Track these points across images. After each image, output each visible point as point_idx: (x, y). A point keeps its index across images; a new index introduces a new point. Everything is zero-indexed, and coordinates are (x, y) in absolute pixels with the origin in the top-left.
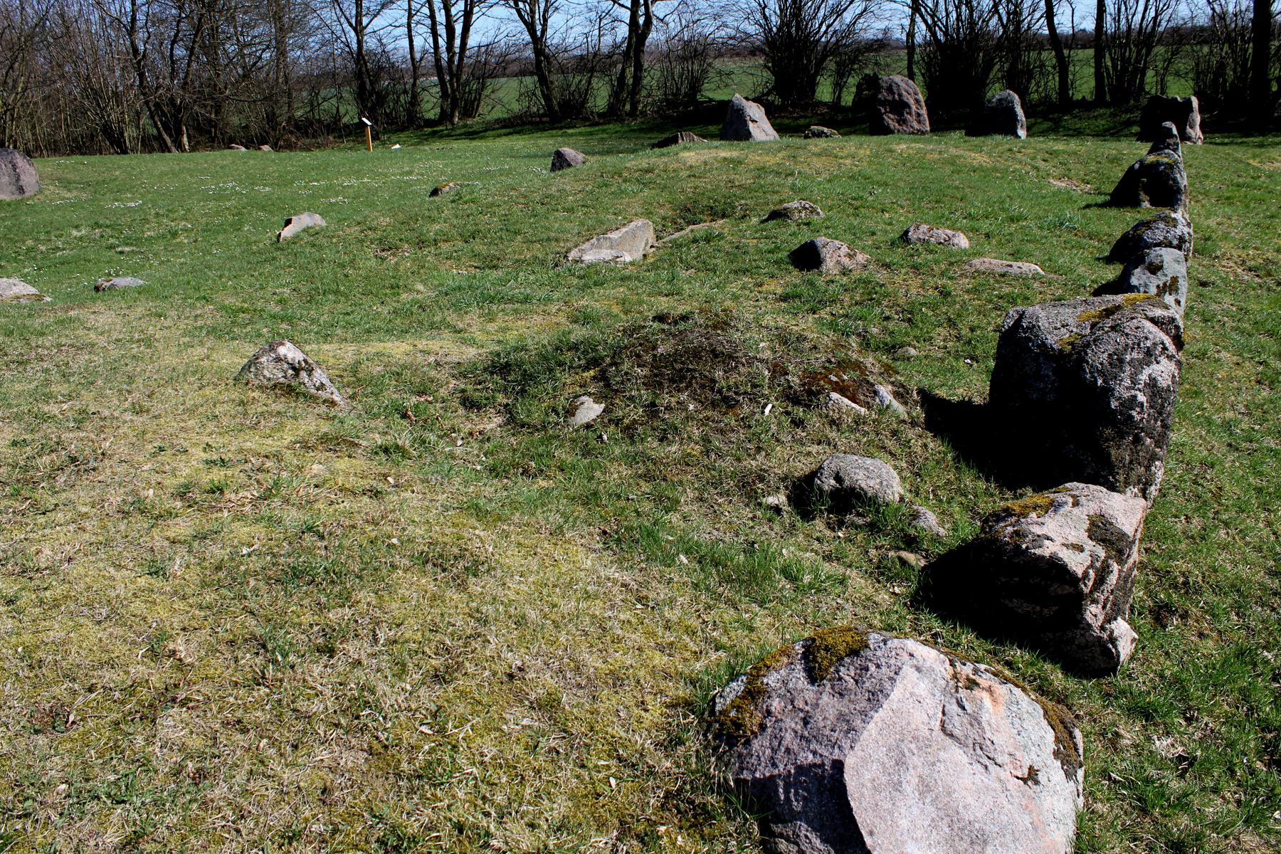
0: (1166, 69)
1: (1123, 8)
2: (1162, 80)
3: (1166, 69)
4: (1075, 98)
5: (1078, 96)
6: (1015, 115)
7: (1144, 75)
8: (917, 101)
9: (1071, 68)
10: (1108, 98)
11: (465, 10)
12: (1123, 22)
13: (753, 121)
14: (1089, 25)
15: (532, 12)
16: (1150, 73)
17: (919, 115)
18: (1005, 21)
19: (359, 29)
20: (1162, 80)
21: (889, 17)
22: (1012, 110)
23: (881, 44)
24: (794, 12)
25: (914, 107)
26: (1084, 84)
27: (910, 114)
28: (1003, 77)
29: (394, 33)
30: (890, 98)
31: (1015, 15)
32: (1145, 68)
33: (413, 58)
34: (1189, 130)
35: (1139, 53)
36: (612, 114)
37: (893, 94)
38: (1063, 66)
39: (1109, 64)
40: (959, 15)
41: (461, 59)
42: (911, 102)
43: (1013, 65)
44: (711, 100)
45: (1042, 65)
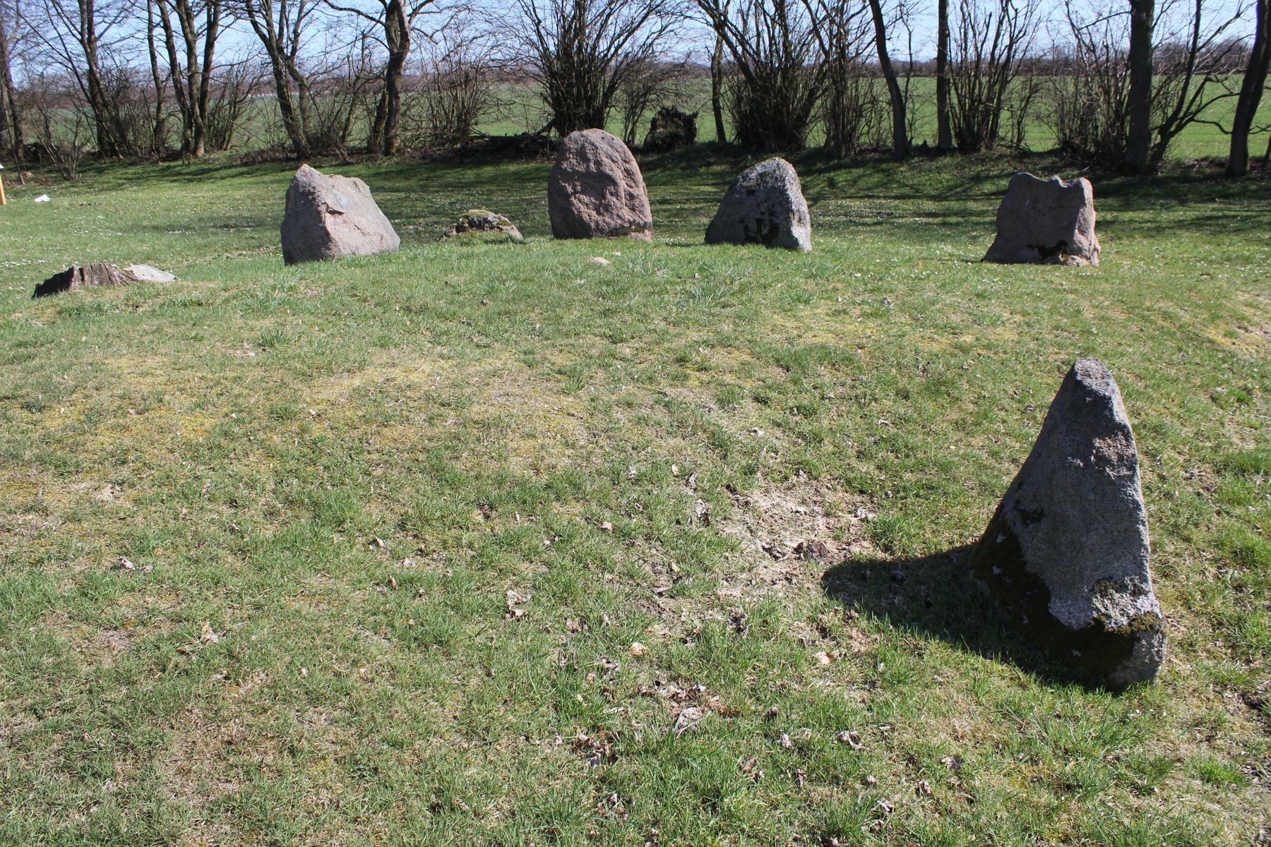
0: (1024, 109)
1: (970, 33)
2: (1019, 123)
3: (1024, 109)
4: (914, 142)
5: (918, 141)
6: (787, 200)
7: (997, 116)
8: (629, 173)
9: (909, 105)
10: (954, 143)
11: (209, 22)
12: (971, 50)
13: (333, 213)
14: (928, 53)
15: (269, 24)
16: (1004, 115)
17: (632, 197)
18: (827, 47)
19: (89, 40)
20: (1019, 123)
21: (689, 40)
22: (782, 193)
23: (681, 69)
24: (573, 29)
25: (623, 184)
26: (925, 129)
27: (616, 195)
28: (825, 116)
29: (130, 47)
30: (582, 168)
31: (840, 38)
32: (999, 108)
33: (156, 79)
34: (1078, 236)
35: (991, 87)
36: (367, 152)
37: (586, 160)
38: (899, 103)
39: (955, 101)
40: (772, 38)
41: (205, 80)
42: (618, 174)
43: (837, 101)
44: (483, 136)
45: (874, 101)
